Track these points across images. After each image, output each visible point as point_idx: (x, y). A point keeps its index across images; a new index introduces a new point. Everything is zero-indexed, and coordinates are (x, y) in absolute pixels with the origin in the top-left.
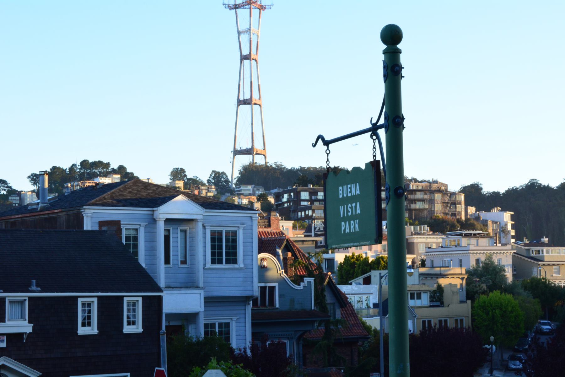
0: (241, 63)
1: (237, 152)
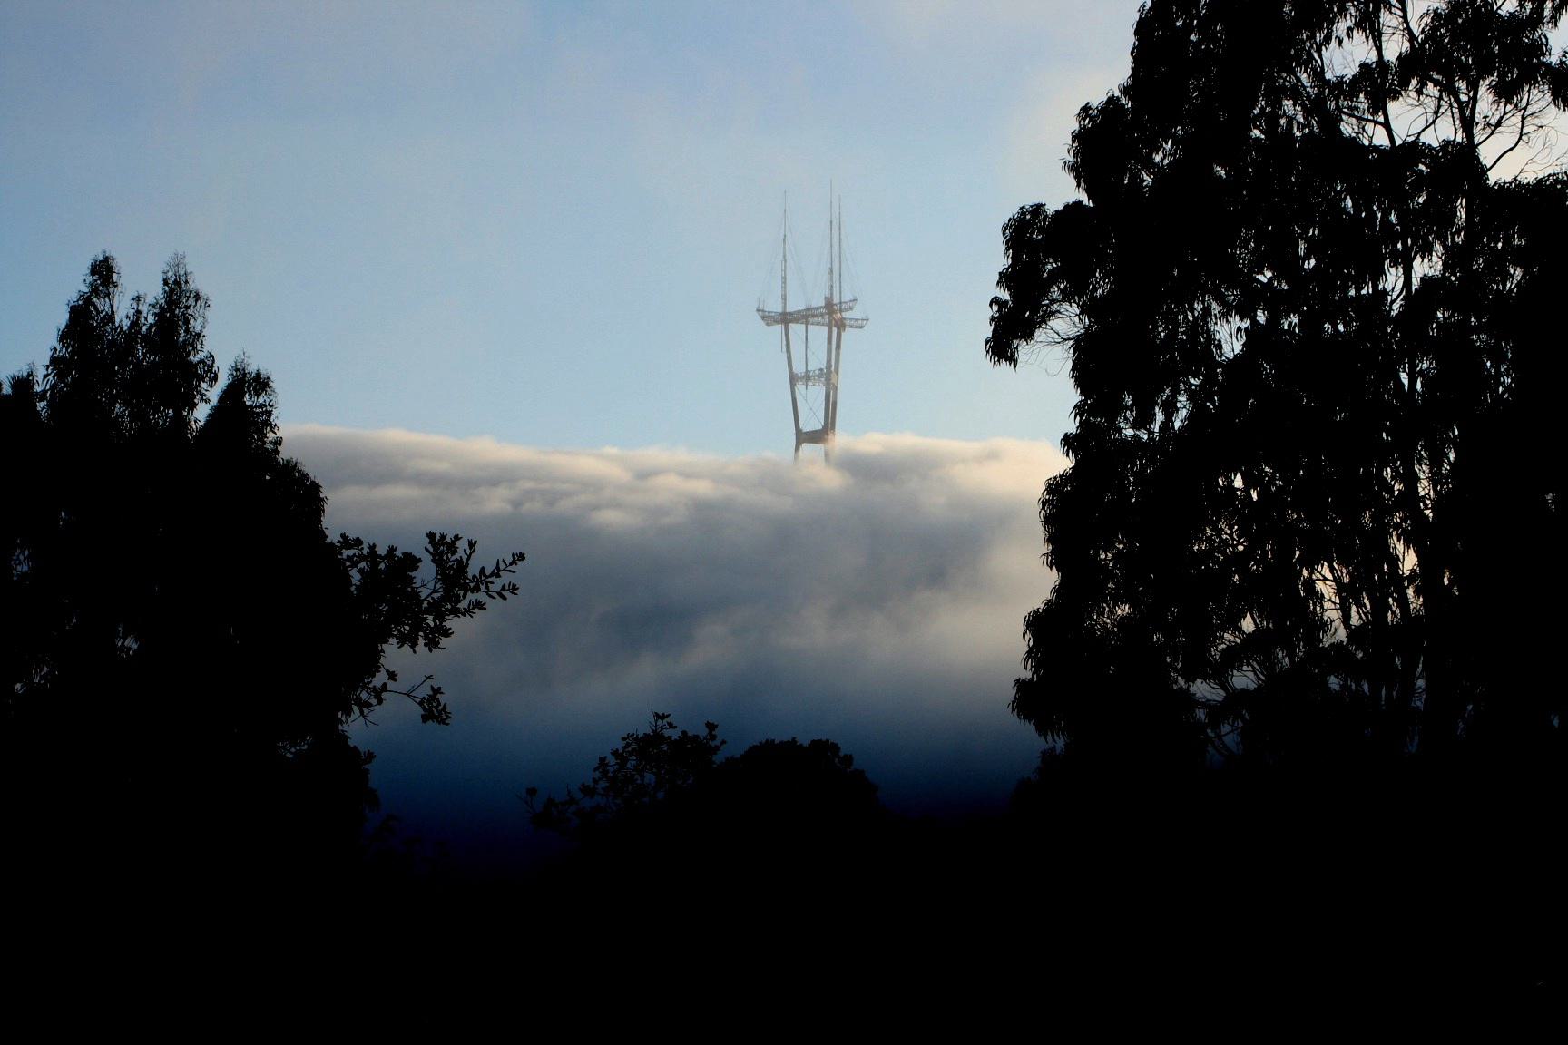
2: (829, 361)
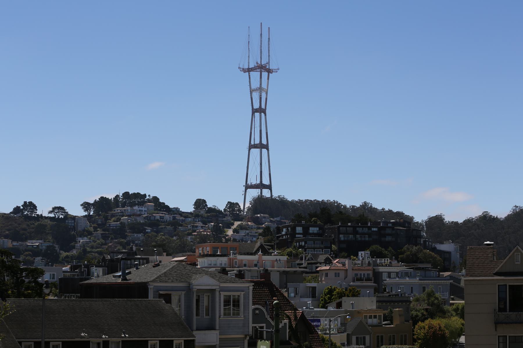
0: (252, 115)
1: (248, 187)
2: (261, 84)
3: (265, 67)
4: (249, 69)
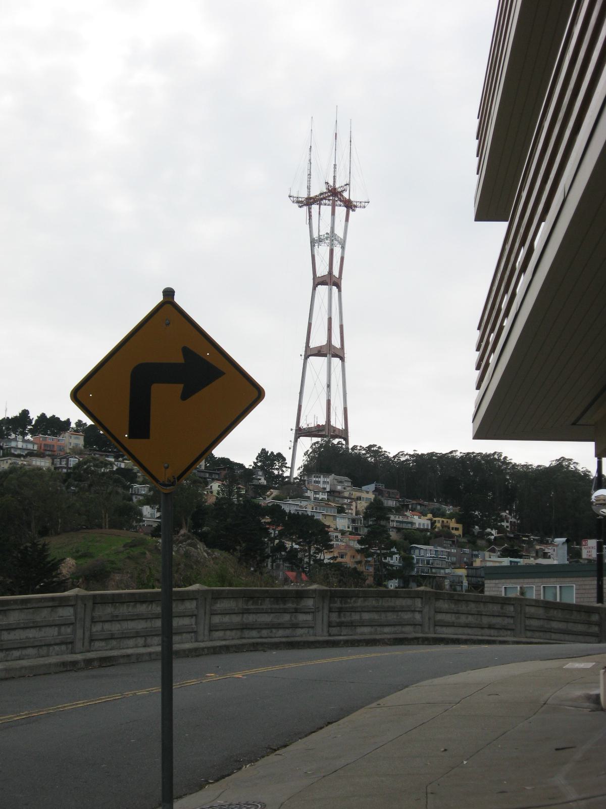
3: (340, 193)
4: (309, 199)
